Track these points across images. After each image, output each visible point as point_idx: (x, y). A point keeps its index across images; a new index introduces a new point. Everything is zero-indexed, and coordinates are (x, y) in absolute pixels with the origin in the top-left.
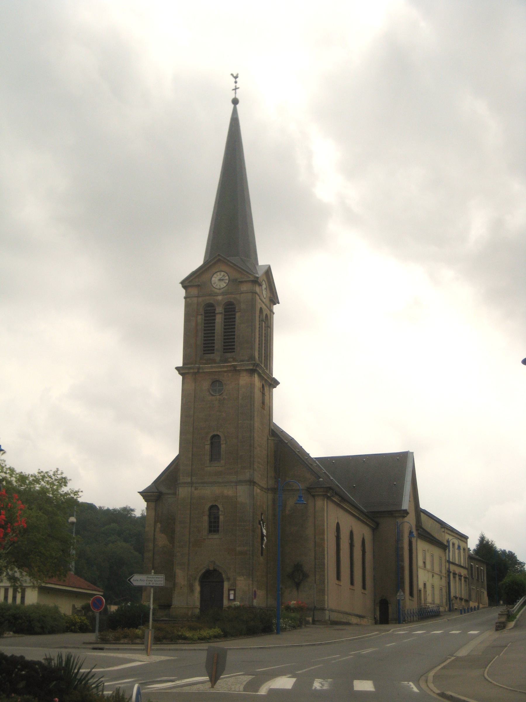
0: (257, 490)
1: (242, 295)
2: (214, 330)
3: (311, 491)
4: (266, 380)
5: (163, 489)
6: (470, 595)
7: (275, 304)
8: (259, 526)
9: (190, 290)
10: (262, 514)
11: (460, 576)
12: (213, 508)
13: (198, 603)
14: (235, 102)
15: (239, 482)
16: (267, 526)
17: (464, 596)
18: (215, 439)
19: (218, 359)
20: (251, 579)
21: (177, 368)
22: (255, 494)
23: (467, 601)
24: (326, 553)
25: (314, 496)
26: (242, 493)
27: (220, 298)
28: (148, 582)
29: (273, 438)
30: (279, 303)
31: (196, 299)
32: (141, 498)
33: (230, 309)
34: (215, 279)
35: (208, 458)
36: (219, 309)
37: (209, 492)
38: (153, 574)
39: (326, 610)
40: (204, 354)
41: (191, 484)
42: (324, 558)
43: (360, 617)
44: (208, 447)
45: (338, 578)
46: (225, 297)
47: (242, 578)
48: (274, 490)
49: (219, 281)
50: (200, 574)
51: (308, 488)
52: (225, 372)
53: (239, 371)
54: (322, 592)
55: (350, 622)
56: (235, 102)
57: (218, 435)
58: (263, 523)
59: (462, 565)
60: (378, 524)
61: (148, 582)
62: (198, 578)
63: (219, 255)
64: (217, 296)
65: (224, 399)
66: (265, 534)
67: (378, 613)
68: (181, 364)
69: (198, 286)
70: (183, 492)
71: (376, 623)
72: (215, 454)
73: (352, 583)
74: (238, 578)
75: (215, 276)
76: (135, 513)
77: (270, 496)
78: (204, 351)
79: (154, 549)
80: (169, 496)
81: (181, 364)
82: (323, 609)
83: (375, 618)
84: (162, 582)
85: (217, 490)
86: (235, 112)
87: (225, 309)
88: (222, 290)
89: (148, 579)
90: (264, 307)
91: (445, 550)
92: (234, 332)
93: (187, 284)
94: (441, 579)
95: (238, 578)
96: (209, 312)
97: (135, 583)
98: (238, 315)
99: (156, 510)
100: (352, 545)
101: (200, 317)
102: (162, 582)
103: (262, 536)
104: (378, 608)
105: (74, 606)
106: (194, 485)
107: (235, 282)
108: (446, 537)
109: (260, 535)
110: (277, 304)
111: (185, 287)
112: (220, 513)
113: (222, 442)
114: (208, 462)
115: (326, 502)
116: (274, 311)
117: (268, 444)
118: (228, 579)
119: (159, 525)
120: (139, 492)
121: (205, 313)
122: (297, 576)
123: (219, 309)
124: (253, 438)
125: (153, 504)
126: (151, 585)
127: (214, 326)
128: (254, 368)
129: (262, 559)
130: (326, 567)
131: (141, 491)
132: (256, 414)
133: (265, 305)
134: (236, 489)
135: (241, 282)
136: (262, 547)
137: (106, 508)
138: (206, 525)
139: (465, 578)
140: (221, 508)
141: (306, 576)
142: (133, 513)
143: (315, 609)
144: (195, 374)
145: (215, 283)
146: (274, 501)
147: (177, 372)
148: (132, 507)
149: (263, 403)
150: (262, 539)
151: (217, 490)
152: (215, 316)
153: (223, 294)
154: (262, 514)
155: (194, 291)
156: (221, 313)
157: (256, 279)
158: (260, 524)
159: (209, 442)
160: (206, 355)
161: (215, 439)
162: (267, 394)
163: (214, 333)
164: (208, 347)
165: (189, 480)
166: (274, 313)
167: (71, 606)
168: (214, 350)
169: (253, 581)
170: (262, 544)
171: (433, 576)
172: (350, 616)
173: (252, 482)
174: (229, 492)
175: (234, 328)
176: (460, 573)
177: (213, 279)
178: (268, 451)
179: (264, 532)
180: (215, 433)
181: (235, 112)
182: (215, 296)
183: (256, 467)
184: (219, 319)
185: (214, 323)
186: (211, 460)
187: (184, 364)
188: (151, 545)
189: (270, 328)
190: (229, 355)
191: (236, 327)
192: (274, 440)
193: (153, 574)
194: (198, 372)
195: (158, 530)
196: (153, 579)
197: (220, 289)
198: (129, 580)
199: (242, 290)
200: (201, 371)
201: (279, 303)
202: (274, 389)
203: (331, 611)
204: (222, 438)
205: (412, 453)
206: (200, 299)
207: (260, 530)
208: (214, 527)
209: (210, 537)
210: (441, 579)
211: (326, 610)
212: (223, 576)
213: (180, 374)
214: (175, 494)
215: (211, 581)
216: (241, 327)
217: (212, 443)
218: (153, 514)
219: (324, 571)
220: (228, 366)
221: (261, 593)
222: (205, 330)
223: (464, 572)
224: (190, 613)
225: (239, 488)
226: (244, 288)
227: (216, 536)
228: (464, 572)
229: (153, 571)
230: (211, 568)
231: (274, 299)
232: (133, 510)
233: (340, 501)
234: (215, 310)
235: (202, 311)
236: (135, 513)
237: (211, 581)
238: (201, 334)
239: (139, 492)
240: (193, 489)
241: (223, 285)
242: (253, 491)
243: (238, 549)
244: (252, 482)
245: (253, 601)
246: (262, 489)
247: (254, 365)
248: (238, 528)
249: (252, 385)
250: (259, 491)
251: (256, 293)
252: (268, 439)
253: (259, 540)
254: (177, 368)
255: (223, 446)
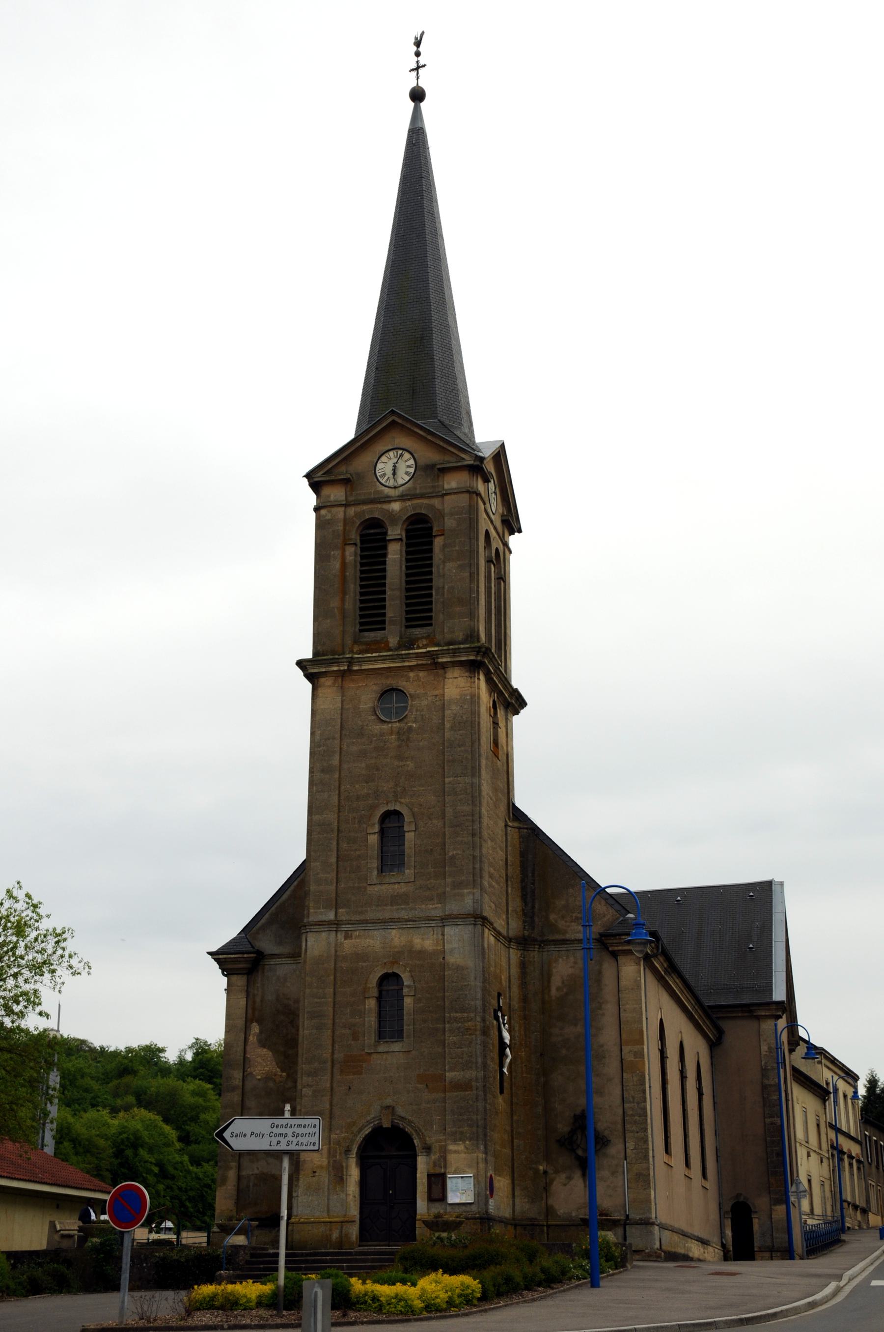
0: (490, 939)
1: (447, 498)
2: (384, 577)
3: (610, 943)
4: (500, 694)
5: (267, 944)
6: (868, 1201)
7: (512, 533)
8: (495, 1022)
9: (326, 491)
10: (499, 995)
11: (851, 1157)
12: (390, 980)
13: (354, 1211)
14: (417, 95)
15: (445, 920)
16: (509, 1022)
17: (860, 1201)
18: (391, 819)
19: (393, 641)
20: (482, 1147)
21: (301, 664)
22: (486, 946)
23: (865, 1211)
24: (647, 1085)
25: (615, 955)
26: (456, 943)
27: (396, 506)
28: (274, 1140)
29: (516, 824)
30: (520, 531)
31: (342, 509)
32: (216, 965)
33: (420, 531)
34: (384, 466)
35: (375, 864)
36: (395, 531)
37: (374, 941)
38: (287, 1115)
39: (653, 1224)
40: (361, 631)
41: (336, 925)
42: (645, 1101)
43: (704, 1242)
44: (374, 839)
45: (667, 1150)
46: (409, 503)
47: (461, 1147)
48: (523, 942)
49: (395, 469)
50: (359, 1139)
51: (601, 935)
52: (411, 668)
53: (444, 666)
54: (643, 1179)
55: (691, 1255)
56: (417, 95)
57: (397, 813)
58: (503, 1016)
59: (852, 1134)
60: (720, 1032)
61: (274, 1140)
62: (355, 1151)
63: (393, 412)
64: (390, 502)
65: (410, 729)
66: (507, 1041)
67: (729, 1233)
68: (308, 654)
69: (346, 482)
70: (316, 944)
71: (726, 1258)
72: (391, 857)
73: (687, 1164)
74: (451, 1147)
75: (384, 459)
76: (166, 1055)
77: (515, 955)
78: (361, 624)
79: (243, 1085)
80: (278, 961)
81: (308, 654)
82: (647, 1223)
83: (723, 1246)
84: (315, 1139)
85: (397, 937)
86: (417, 115)
87: (407, 531)
88: (401, 489)
89: (275, 1130)
90: (493, 533)
91: (824, 1101)
92: (431, 580)
93: (318, 478)
94: (822, 1162)
95: (451, 1147)
96: (372, 538)
97: (238, 1144)
98: (438, 542)
99: (248, 993)
100: (683, 1077)
101: (350, 551)
102: (315, 1139)
103: (502, 1045)
104: (728, 1223)
105: (52, 1225)
106: (344, 928)
107: (429, 471)
108: (824, 1075)
109: (496, 1042)
110: (516, 534)
111: (316, 486)
112: (405, 990)
113: (406, 828)
114: (375, 872)
115: (642, 968)
116: (511, 546)
117: (506, 834)
118: (428, 1149)
119: (255, 1028)
120: (209, 953)
121: (362, 542)
122: (578, 1142)
123: (395, 531)
124: (480, 817)
125: (240, 981)
126: (283, 1147)
127: (384, 570)
128: (479, 658)
129: (501, 1102)
130: (649, 1120)
131: (214, 949)
132: (484, 762)
133: (495, 528)
134: (443, 935)
135: (444, 471)
136: (502, 1073)
137: (112, 1049)
138: (372, 1020)
139: (859, 1161)
140: (407, 981)
141: (602, 1142)
142: (162, 1055)
143: (626, 1223)
144: (342, 674)
145: (384, 475)
146: (523, 965)
147: (300, 673)
148: (160, 1045)
149: (496, 743)
150: (502, 1055)
151: (397, 937)
152: (385, 548)
153: (402, 498)
154: (499, 995)
155: (336, 493)
156: (401, 540)
157: (478, 463)
158: (496, 1018)
159: (376, 828)
160: (366, 634)
161: (391, 819)
162: (502, 724)
163: (384, 585)
164: (371, 615)
165: (331, 916)
166: (510, 552)
167: (46, 1228)
168: (384, 622)
169: (486, 1153)
170: (501, 1066)
171: (809, 1155)
172: (689, 1240)
173: (479, 919)
174: (424, 941)
175: (431, 573)
176: (849, 1150)
177: (379, 466)
178: (507, 851)
179: (506, 1036)
180: (391, 807)
181: (417, 115)
182: (384, 502)
183: (486, 883)
184: (395, 553)
185: (384, 563)
186: (381, 870)
187: (316, 653)
188: (237, 1075)
189: (504, 582)
190: (417, 632)
191: (434, 570)
192: (519, 828)
193: (287, 1115)
194: (349, 671)
195: (252, 1039)
196: (289, 1131)
197: (395, 488)
198: (220, 1135)
199: (446, 487)
200: (355, 668)
201: (520, 531)
202: (515, 718)
203: (663, 1227)
204: (407, 819)
205: (782, 884)
206: (351, 511)
207: (497, 1033)
208: (390, 1026)
209: (381, 1049)
210: (822, 1162)
211: (653, 1224)
212: (415, 1141)
213: (309, 677)
214: (296, 955)
215: (388, 1153)
216: (446, 570)
217: (382, 832)
218: (243, 1002)
219: (646, 1130)
220: (418, 655)
221: (502, 1183)
222: (362, 579)
223: (855, 1150)
224: (335, 1235)
225: (450, 931)
226: (452, 482)
227: (396, 1047)
228: (855, 1150)
229: (288, 1107)
230: (386, 1124)
231: (511, 523)
232: (162, 1050)
233: (666, 970)
234: (386, 533)
235: (355, 536)
236: (166, 1055)
237: (388, 1153)
238: (353, 588)
239: (209, 953)
240: (341, 936)
241: (403, 478)
242: (483, 938)
243: (449, 1075)
244: (479, 919)
245: (487, 1203)
246: (498, 934)
247: (478, 650)
248: (447, 1026)
249: (474, 699)
250: (492, 939)
251: (478, 494)
252: (506, 826)
253: (495, 1055)
254: (301, 664)
255: (409, 837)
